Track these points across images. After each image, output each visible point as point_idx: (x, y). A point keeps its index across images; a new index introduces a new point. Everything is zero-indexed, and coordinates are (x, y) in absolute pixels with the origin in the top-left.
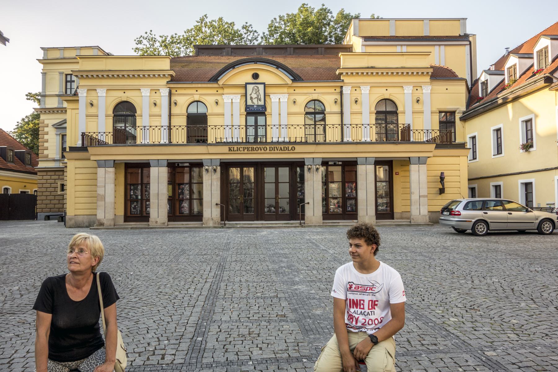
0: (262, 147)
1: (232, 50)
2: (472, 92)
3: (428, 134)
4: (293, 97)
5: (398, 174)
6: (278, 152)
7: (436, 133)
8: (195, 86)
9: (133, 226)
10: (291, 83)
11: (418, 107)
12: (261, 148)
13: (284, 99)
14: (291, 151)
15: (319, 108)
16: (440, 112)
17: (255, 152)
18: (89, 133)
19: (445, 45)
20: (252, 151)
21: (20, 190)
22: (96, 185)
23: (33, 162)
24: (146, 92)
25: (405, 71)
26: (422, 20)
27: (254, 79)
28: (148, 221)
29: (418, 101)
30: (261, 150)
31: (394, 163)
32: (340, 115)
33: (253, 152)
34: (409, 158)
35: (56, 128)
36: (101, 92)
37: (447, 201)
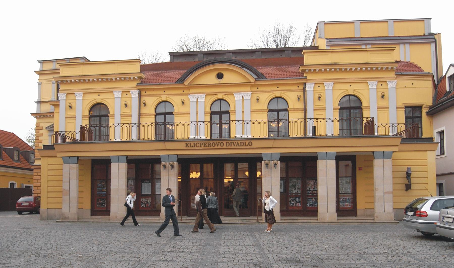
0: (219, 143)
1: (205, 56)
2: (438, 88)
3: (394, 128)
4: (256, 95)
5: (362, 170)
6: (235, 147)
7: (402, 127)
8: (333, 78)
9: (95, 220)
10: (254, 82)
11: (383, 103)
12: (218, 143)
13: (248, 96)
14: (249, 147)
15: (282, 106)
16: (406, 107)
17: (212, 147)
18: (62, 132)
19: (410, 43)
20: (208, 146)
21: (25, 185)
22: (62, 181)
23: (21, 159)
24: (117, 94)
25: (369, 67)
26: (386, 21)
27: (219, 79)
28: (109, 215)
29: (383, 96)
30: (218, 146)
31: (356, 156)
32: (303, 112)
33: (210, 148)
34: (373, 152)
35: (48, 130)
36: (79, 96)
37: (415, 197)
